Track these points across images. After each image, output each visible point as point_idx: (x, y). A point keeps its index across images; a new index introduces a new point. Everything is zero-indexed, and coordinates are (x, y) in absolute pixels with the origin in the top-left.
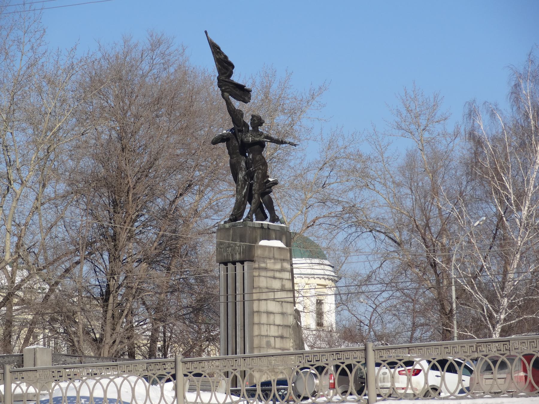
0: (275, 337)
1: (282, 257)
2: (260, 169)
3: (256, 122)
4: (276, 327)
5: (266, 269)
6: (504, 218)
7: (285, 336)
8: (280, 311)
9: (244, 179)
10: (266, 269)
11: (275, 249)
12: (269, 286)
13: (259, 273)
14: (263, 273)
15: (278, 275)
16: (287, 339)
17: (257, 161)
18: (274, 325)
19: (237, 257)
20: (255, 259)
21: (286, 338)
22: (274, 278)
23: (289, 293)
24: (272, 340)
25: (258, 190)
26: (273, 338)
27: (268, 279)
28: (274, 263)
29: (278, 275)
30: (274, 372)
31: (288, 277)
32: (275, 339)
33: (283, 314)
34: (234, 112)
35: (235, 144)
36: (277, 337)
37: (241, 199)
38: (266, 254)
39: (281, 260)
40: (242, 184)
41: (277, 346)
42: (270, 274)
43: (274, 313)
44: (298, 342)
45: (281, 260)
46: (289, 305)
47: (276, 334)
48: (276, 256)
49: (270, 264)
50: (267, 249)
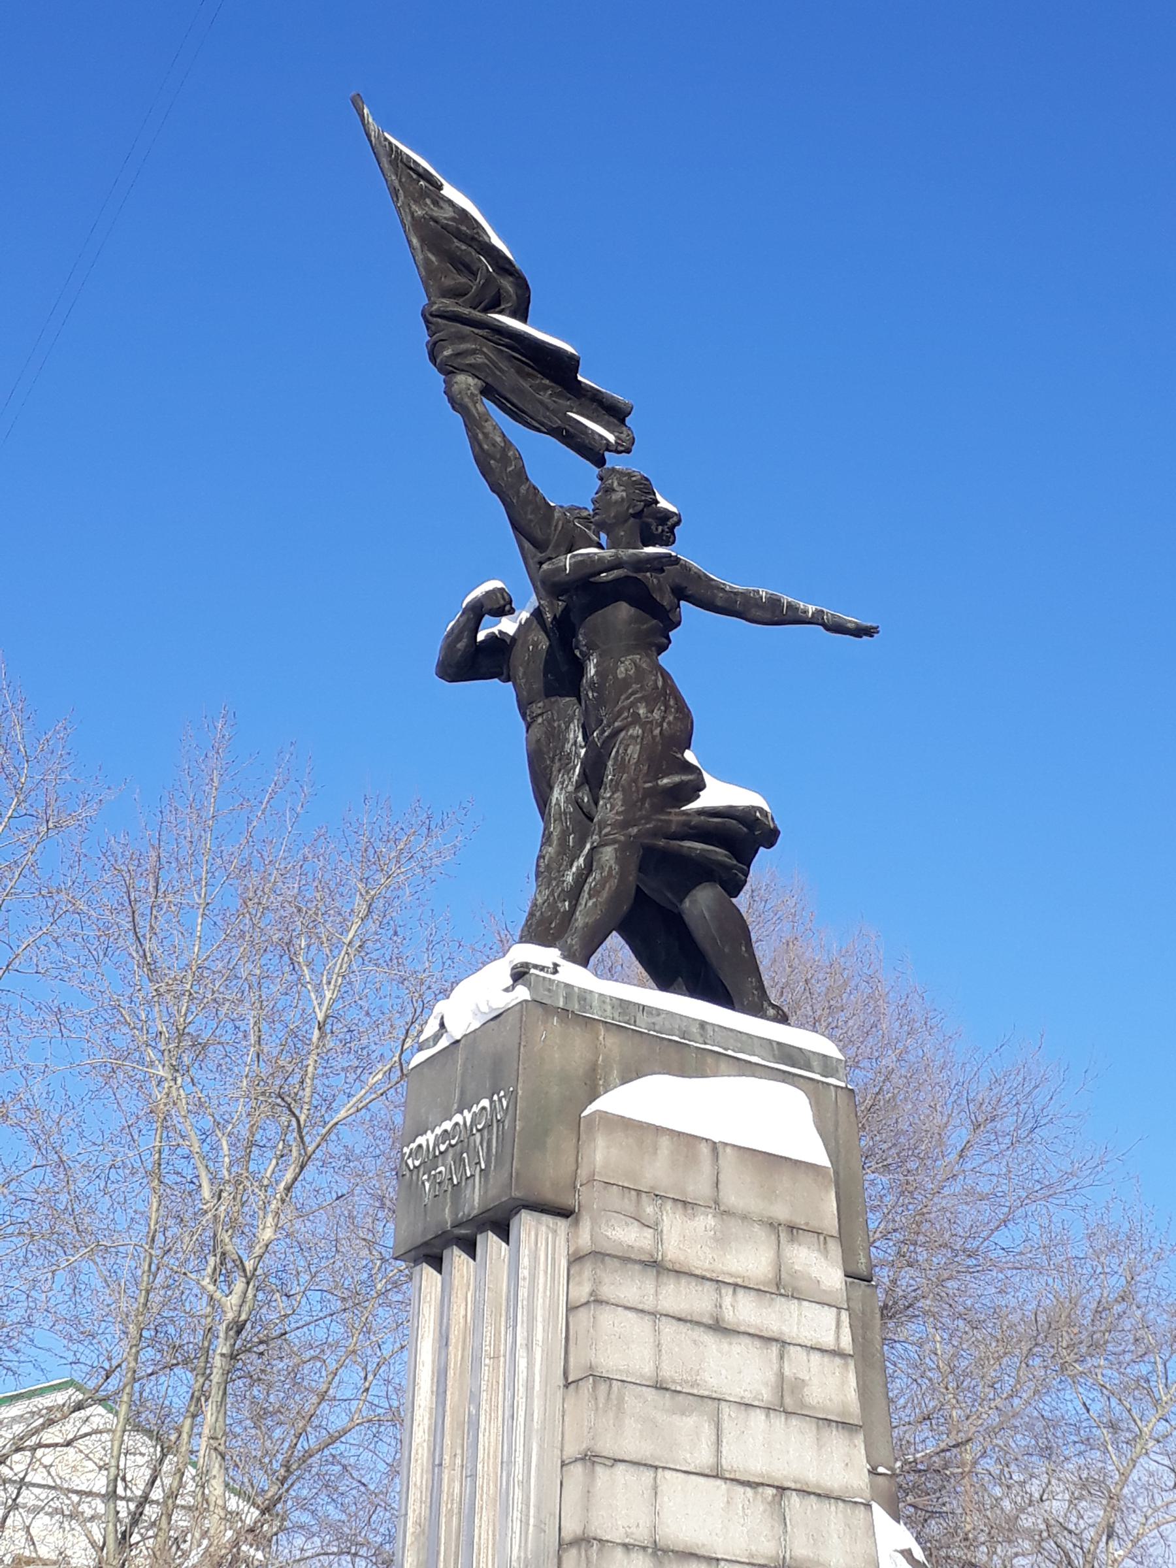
1: (781, 1212)
3: (620, 494)
9: (578, 804)
10: (656, 1266)
11: (728, 1160)
12: (668, 1372)
13: (597, 1282)
14: (632, 1288)
15: (743, 1310)
17: (626, 683)
20: (587, 1197)
22: (718, 1327)
23: (837, 1441)
25: (624, 825)
27: (669, 1329)
28: (721, 1241)
29: (743, 1310)
34: (504, 460)
37: (553, 906)
38: (658, 1170)
39: (773, 1226)
40: (564, 834)
42: (677, 1297)
45: (773, 1226)
46: (833, 1514)
48: (732, 1198)
49: (684, 1237)
50: (665, 1142)
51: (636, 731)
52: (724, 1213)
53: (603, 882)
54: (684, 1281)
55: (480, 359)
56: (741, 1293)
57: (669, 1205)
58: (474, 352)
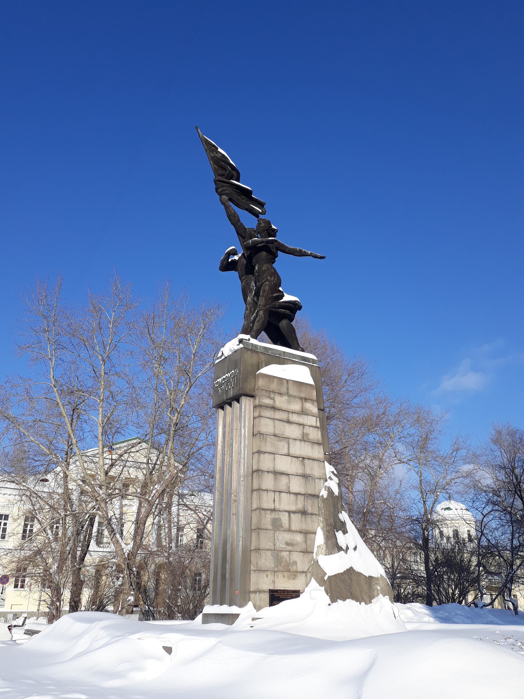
0: (289, 512)
1: (303, 395)
2: (267, 280)
3: (263, 225)
4: (292, 497)
5: (274, 408)
6: (493, 585)
7: (310, 510)
8: (300, 471)
9: (254, 301)
10: (274, 408)
13: (260, 412)
15: (294, 418)
16: (314, 517)
17: (265, 271)
18: (289, 493)
19: (231, 394)
21: (312, 514)
22: (289, 422)
23: (316, 447)
24: (284, 518)
25: (265, 306)
26: (287, 514)
27: (277, 422)
28: (289, 402)
29: (294, 418)
30: (289, 571)
31: (314, 424)
32: (289, 515)
33: (305, 476)
35: (243, 262)
36: (294, 512)
37: (248, 325)
38: (274, 386)
39: (301, 398)
40: (251, 308)
41: (293, 528)
43: (288, 475)
44: (332, 521)
45: (301, 398)
46: (316, 464)
47: (293, 508)
51: (267, 283)
52: (289, 396)
53: (260, 319)
54: (280, 411)
55: (228, 192)
56: (294, 414)
57: (277, 394)
58: (226, 190)
